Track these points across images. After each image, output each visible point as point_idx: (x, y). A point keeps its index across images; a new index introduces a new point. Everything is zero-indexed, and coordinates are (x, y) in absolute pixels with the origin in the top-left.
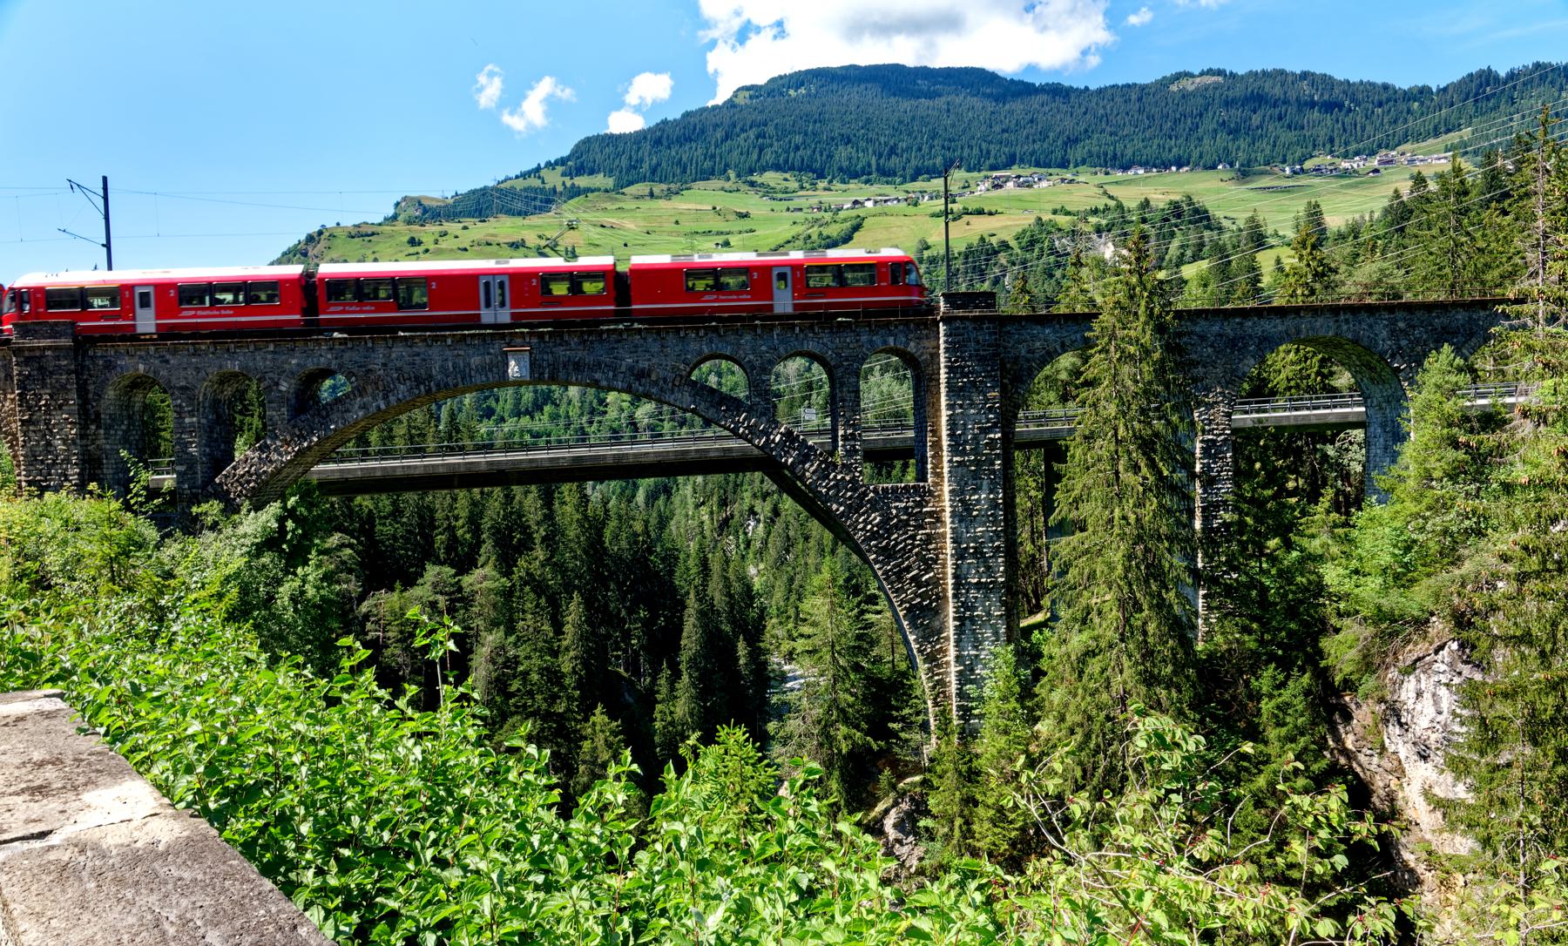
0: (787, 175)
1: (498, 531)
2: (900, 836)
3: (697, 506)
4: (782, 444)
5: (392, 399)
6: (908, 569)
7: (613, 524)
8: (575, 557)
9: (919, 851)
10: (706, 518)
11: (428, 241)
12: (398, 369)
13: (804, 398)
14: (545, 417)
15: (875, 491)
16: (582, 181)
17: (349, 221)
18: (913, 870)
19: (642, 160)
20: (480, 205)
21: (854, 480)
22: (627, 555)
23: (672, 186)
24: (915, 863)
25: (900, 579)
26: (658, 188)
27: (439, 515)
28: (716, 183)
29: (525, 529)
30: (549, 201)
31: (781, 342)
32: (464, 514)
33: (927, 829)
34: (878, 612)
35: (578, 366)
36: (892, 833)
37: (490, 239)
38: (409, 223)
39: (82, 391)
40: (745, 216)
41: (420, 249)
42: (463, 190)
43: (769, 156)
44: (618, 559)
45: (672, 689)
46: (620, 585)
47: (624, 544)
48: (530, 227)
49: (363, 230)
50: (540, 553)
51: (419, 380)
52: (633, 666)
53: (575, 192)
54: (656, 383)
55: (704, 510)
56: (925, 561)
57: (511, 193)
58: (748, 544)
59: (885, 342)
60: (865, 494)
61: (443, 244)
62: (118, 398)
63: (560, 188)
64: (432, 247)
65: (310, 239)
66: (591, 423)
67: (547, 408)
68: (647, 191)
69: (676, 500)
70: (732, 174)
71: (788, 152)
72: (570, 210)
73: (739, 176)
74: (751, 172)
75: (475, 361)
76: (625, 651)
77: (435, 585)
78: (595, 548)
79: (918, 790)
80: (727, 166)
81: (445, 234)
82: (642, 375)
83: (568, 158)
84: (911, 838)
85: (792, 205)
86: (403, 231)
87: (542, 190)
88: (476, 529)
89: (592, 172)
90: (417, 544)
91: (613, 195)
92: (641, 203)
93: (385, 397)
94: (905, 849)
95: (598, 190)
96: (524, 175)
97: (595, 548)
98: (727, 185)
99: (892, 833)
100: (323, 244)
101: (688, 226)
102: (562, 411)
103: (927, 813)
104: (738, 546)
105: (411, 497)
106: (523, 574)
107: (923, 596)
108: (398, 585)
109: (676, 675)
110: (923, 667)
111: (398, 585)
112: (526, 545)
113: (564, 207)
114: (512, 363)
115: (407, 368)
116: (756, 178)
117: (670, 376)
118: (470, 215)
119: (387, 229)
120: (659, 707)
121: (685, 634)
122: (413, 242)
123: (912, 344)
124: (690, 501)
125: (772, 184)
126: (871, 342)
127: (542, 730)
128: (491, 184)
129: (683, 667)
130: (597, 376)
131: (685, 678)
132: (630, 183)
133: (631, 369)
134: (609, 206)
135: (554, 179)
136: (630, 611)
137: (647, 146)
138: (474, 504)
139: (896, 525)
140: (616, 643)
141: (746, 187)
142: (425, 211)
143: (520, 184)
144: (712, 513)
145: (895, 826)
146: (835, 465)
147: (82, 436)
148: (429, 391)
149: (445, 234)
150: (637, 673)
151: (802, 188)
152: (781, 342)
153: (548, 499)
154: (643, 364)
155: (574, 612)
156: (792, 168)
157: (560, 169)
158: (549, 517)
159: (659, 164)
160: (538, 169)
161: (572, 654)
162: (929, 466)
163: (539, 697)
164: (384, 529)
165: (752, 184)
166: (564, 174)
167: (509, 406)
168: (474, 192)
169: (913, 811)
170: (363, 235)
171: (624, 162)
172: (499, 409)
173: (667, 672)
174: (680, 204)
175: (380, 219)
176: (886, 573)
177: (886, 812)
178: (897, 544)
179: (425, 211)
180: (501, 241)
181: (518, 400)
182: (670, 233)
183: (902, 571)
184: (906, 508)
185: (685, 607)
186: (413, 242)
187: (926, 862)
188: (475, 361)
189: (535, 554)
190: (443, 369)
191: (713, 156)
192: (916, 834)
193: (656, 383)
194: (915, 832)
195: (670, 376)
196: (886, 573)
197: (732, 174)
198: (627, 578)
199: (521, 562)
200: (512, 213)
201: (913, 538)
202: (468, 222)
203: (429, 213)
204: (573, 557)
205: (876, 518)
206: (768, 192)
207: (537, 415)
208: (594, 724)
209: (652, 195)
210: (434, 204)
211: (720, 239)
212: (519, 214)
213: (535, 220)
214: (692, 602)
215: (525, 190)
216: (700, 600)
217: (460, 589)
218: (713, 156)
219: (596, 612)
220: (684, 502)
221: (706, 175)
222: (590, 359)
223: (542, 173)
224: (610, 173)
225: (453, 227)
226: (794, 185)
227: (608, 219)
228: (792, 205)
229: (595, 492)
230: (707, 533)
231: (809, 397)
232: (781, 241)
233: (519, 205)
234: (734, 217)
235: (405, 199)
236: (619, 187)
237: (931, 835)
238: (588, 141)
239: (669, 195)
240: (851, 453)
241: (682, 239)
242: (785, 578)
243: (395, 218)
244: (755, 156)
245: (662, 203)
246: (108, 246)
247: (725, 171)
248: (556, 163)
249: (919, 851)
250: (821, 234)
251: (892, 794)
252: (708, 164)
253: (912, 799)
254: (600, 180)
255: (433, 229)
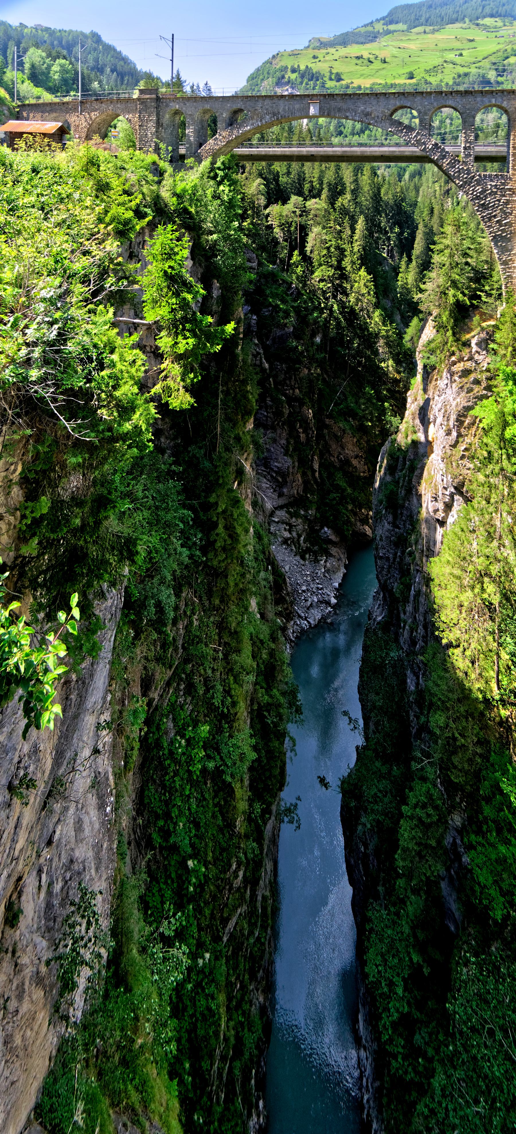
0: (497, 19)
1: (330, 185)
2: (479, 350)
3: (434, 182)
4: (432, 149)
5: (264, 121)
6: (495, 216)
7: (386, 186)
8: (367, 200)
9: (488, 360)
10: (438, 188)
11: (321, 57)
12: (267, 109)
13: (494, 132)
14: (365, 136)
15: (480, 176)
16: (392, 27)
17: (289, 49)
18: (484, 369)
19: (421, 16)
20: (344, 40)
21: (468, 169)
22: (391, 202)
23: (436, 27)
24: (486, 365)
25: (490, 219)
26: (428, 29)
27: (307, 175)
28: (458, 25)
29: (343, 185)
30: (376, 37)
31: (435, 100)
32: (316, 176)
33: (493, 349)
34: (484, 238)
35: (339, 110)
36: (475, 348)
37: (347, 55)
38: (314, 49)
39: (158, 115)
40: (472, 41)
41: (317, 60)
42: (338, 34)
43: (487, 10)
44: (387, 204)
45: (407, 267)
46: (387, 215)
47: (390, 196)
48: (366, 49)
49: (295, 53)
50: (348, 196)
51: (274, 114)
52: (390, 252)
53: (388, 32)
54: (374, 118)
55: (437, 185)
56: (505, 213)
57: (359, 34)
58: (458, 204)
59: (490, 101)
60: (474, 177)
61: (328, 58)
62: (170, 118)
63: (381, 31)
64: (322, 59)
65: (274, 57)
66: (386, 139)
67: (367, 132)
68: (423, 30)
69: (424, 178)
70: (467, 20)
71: (498, 7)
72: (384, 41)
73: (471, 21)
74: (477, 18)
75: (297, 106)
76: (388, 247)
77: (295, 204)
78: (376, 197)
79: (491, 329)
80: (465, 16)
81: (328, 53)
82: (367, 114)
83: (386, 17)
84: (484, 352)
85: (498, 34)
86: (311, 52)
87: (373, 32)
88: (321, 183)
89: (397, 23)
90: (296, 187)
91: (406, 33)
92: (419, 36)
93: (261, 121)
94: (481, 357)
95: (399, 31)
96: (365, 26)
97: (376, 197)
98: (464, 26)
99: (475, 348)
100: (278, 59)
101: (441, 46)
102: (373, 134)
103: (493, 341)
104: (453, 204)
105: (295, 166)
106: (340, 204)
107: (503, 231)
108: (280, 203)
109: (410, 260)
110: (499, 267)
111: (280, 203)
112: (342, 193)
113: (382, 39)
114: (311, 107)
115: (270, 109)
116: (480, 22)
117: (380, 115)
118: (340, 45)
119: (304, 52)
120: (400, 275)
121: (416, 242)
122: (314, 57)
123: (505, 102)
124: (431, 180)
125: (488, 24)
126: (482, 101)
127: (334, 274)
128: (350, 30)
129: (413, 257)
130: (348, 114)
131: (414, 262)
132: (415, 27)
133: (363, 111)
134: (403, 38)
135: (379, 27)
136: (391, 229)
137: (424, 9)
138: (322, 172)
139: (490, 194)
140: (384, 242)
141: (474, 26)
142: (321, 44)
143: (363, 30)
144: (441, 186)
145: (476, 344)
146: (459, 162)
147: (157, 132)
148: (278, 119)
149: (328, 53)
150: (392, 257)
151: (505, 25)
152: (435, 100)
153: (357, 171)
154: (369, 110)
155: (361, 224)
156: (500, 16)
157: (382, 22)
158: (356, 181)
159: (430, 17)
160: (372, 23)
161: (358, 243)
162: (511, 165)
163: (333, 259)
164: (283, 180)
165: (478, 25)
166: (384, 24)
167: (349, 131)
168: (342, 34)
169: (487, 339)
170: (295, 54)
171: (413, 17)
172: (345, 132)
173: (405, 259)
174: (438, 36)
175: (302, 48)
176: (483, 217)
177: (474, 337)
178: (489, 203)
179: (321, 44)
180: (352, 56)
181: (354, 128)
182: (433, 50)
183: (491, 217)
184: (496, 185)
185: (417, 229)
186: (314, 57)
187: (491, 366)
188: (297, 106)
189: (345, 196)
190: (284, 110)
191: (458, 12)
192: (488, 351)
193: (374, 118)
194: (486, 349)
195: (380, 115)
196: (483, 217)
197: (467, 20)
198: (390, 212)
199: (340, 199)
200: (358, 43)
201: (499, 201)
202: (338, 47)
203: (323, 45)
204: (365, 200)
205: (479, 189)
206: (486, 28)
207: (362, 135)
208: (360, 276)
209: (425, 32)
210: (325, 40)
211: (458, 53)
212: (362, 43)
213: (368, 46)
214: (421, 226)
215: (365, 32)
216: (426, 226)
217: (305, 207)
218: (458, 12)
219: (372, 226)
220: (428, 180)
221: (453, 21)
222: (345, 106)
223: (374, 24)
224: (405, 23)
225: (332, 50)
226: (500, 24)
227: (402, 44)
228: (498, 34)
229: (383, 170)
230: (438, 196)
231: (497, 132)
232: (490, 53)
233: (363, 40)
234: (465, 42)
235: (313, 38)
236: (410, 28)
237: (495, 352)
238: (396, 8)
239: (434, 32)
240: (468, 156)
241: (438, 53)
242: (475, 222)
243: (308, 47)
244: (480, 10)
245: (429, 36)
246: (172, 60)
247: (464, 19)
248: (381, 19)
249: (488, 360)
250: (513, 49)
251: (479, 329)
252: (455, 16)
253: (487, 333)
254: (401, 26)
255: (324, 51)
